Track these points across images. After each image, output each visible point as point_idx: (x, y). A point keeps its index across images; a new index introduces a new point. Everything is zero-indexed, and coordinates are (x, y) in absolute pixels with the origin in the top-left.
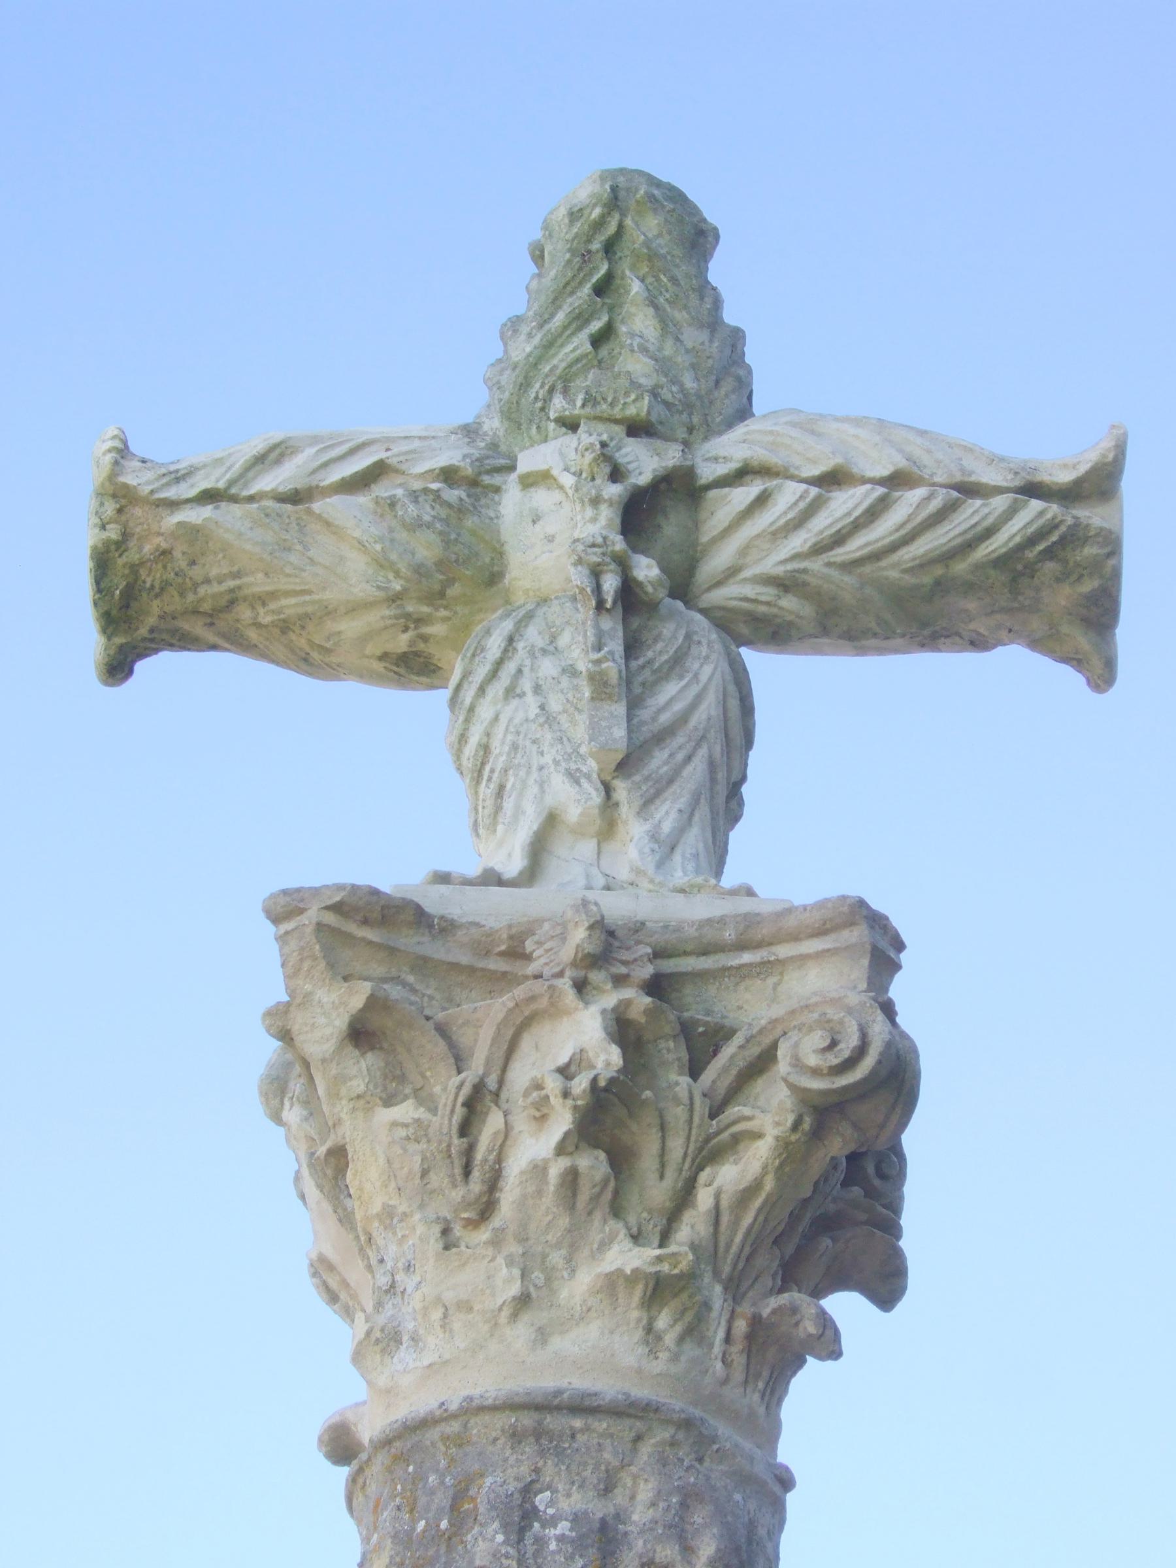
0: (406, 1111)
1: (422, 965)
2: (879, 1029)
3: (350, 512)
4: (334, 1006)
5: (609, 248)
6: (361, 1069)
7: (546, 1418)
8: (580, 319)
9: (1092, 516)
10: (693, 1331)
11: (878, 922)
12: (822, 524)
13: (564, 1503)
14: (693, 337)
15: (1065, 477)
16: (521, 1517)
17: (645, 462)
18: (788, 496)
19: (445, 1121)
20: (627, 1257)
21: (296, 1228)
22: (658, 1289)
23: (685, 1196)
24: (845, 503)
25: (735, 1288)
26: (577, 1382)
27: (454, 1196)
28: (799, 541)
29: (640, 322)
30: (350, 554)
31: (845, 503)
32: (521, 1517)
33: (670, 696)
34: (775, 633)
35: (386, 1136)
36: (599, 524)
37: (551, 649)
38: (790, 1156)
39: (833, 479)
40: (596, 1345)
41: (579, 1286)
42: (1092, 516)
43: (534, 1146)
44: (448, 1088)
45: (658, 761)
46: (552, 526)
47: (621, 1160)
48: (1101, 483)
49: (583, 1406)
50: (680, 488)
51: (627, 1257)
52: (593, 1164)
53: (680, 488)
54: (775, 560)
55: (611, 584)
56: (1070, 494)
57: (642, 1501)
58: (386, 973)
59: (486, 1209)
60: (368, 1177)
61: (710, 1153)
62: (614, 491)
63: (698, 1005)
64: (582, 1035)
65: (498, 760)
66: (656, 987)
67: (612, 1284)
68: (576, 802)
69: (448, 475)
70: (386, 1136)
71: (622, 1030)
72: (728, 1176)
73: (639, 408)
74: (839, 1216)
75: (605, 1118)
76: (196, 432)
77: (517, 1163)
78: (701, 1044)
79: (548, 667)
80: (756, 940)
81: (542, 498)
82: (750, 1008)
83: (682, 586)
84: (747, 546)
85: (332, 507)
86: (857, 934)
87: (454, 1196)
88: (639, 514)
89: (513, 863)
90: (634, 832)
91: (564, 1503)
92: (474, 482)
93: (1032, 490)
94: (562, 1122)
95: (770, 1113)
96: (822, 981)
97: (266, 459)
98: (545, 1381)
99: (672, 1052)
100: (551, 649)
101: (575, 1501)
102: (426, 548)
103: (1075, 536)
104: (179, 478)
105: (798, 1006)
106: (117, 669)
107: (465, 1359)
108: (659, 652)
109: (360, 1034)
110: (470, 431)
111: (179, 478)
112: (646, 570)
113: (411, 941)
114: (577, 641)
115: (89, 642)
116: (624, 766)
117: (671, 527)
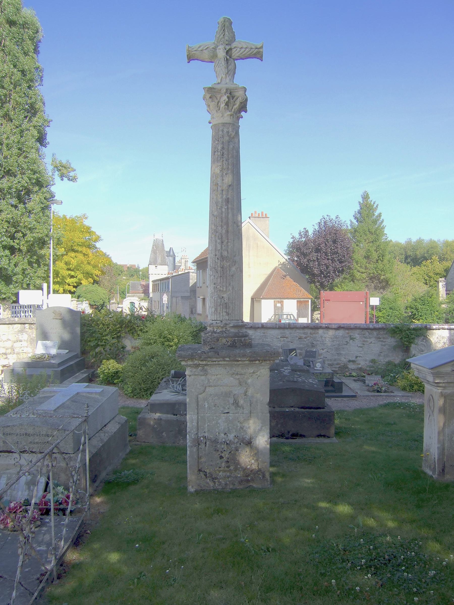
0: (214, 103)
1: (214, 92)
2: (245, 97)
3: (206, 52)
4: (208, 96)
5: (224, 26)
6: (210, 100)
7: (224, 124)
8: (222, 33)
9: (261, 50)
10: (233, 118)
11: (245, 88)
12: (241, 52)
13: (225, 130)
14: (231, 34)
15: (259, 47)
16: (223, 131)
17: (228, 48)
18: (239, 49)
19: (216, 104)
20: (229, 113)
21: (206, 108)
22: (231, 115)
23: (232, 108)
24: (243, 50)
25: (236, 114)
26: (226, 122)
27: (217, 109)
28: (239, 53)
29: (227, 33)
30: (206, 55)
31: (243, 50)
32: (223, 131)
33: (230, 67)
34: (237, 60)
35: (212, 104)
36: (224, 54)
37: (221, 63)
38: (239, 106)
39: (241, 48)
40: (227, 119)
41: (226, 115)
42: (261, 50)
43: (222, 105)
44: (216, 101)
45: (229, 72)
46: (221, 53)
47: (228, 106)
48: (262, 47)
49: (226, 123)
50: (231, 49)
51: (229, 113)
52: (226, 107)
53: (231, 49)
54: (237, 55)
55: (226, 59)
56: (259, 48)
57: (230, 130)
58: (212, 93)
59: (219, 109)
60: (211, 107)
61: (234, 105)
62: (226, 51)
63: (233, 94)
64: (225, 98)
65: (218, 72)
66: (230, 94)
67: (228, 115)
68: (224, 76)
69: (213, 48)
70: (212, 104)
71: (228, 97)
72: (235, 107)
73: (227, 43)
74: (243, 108)
75: (227, 104)
76: (195, 46)
77: (221, 107)
78: (233, 97)
79: (221, 65)
80: (237, 89)
81: (220, 50)
82: (237, 94)
83: (230, 57)
84: (235, 54)
85: (204, 51)
86: (244, 89)
87: (217, 109)
88: (227, 52)
89: (220, 81)
90: (228, 78)
91: (225, 130)
92: (215, 49)
93: (256, 48)
94: (224, 104)
95: (238, 103)
96: (241, 93)
97: (200, 47)
98: (224, 122)
99: (231, 98)
100: (221, 63)
101: (226, 130)
102: (212, 54)
103: (260, 52)
104: (193, 49)
105: (239, 94)
106: (189, 62)
107: (218, 120)
108: (229, 64)
109: (210, 98)
110: (214, 43)
111: (193, 49)
112: (228, 57)
113: (213, 90)
114: (223, 63)
115: (187, 61)
116: (227, 74)
117: (230, 53)
